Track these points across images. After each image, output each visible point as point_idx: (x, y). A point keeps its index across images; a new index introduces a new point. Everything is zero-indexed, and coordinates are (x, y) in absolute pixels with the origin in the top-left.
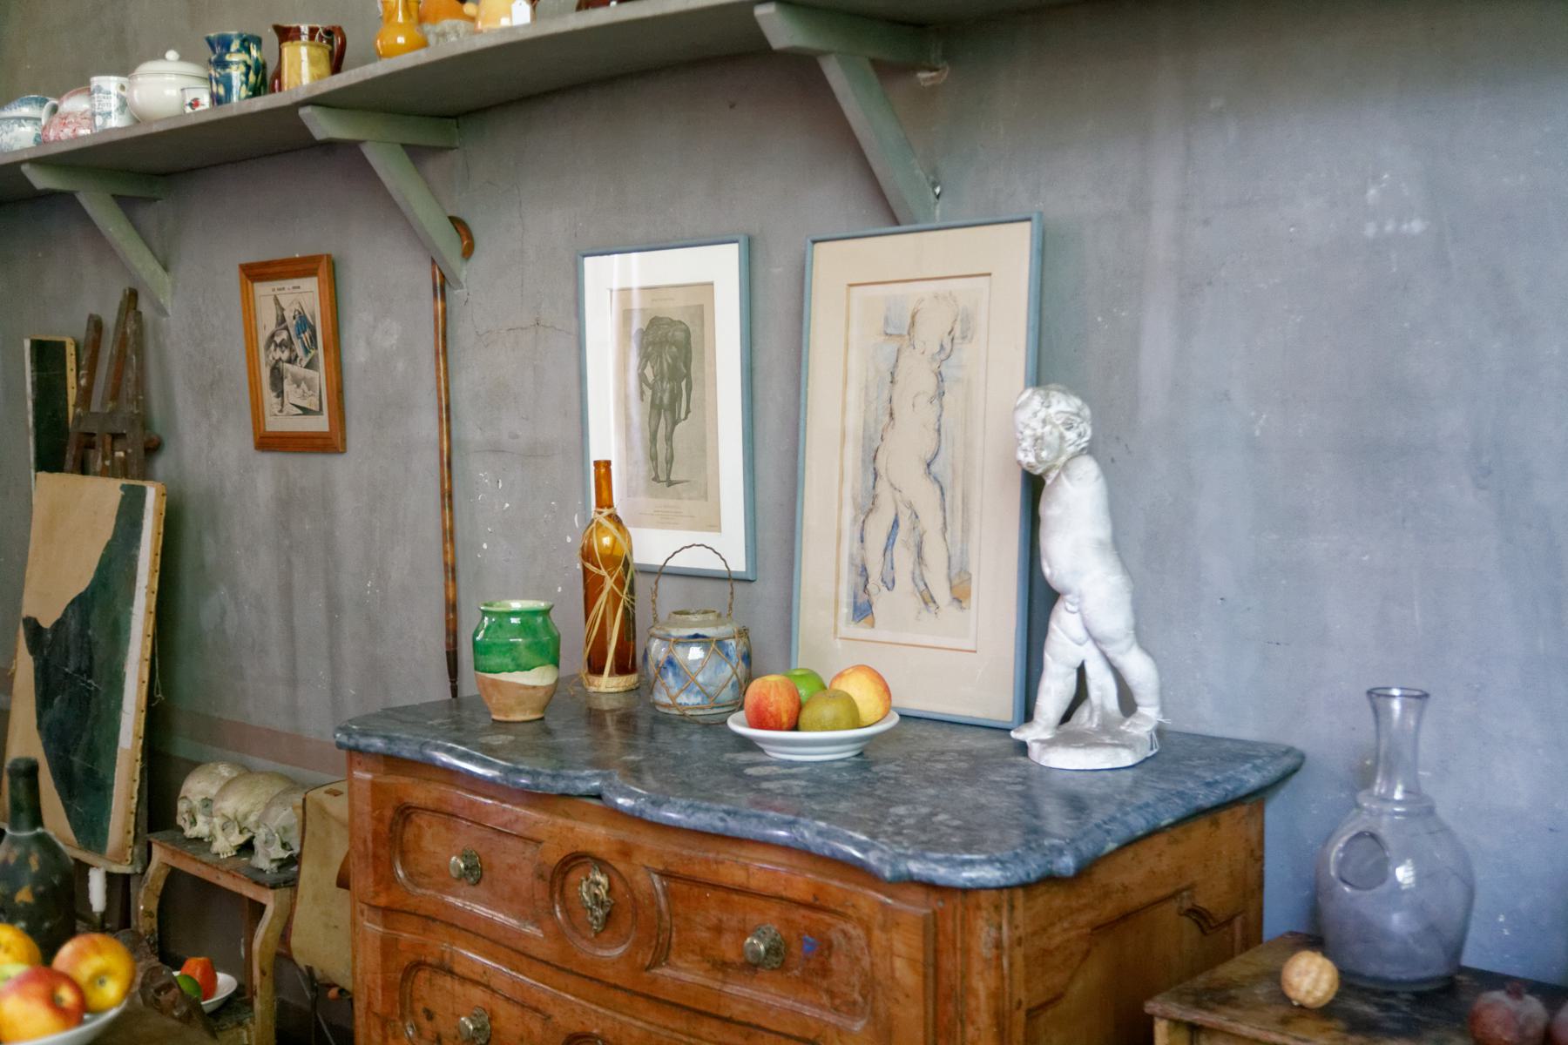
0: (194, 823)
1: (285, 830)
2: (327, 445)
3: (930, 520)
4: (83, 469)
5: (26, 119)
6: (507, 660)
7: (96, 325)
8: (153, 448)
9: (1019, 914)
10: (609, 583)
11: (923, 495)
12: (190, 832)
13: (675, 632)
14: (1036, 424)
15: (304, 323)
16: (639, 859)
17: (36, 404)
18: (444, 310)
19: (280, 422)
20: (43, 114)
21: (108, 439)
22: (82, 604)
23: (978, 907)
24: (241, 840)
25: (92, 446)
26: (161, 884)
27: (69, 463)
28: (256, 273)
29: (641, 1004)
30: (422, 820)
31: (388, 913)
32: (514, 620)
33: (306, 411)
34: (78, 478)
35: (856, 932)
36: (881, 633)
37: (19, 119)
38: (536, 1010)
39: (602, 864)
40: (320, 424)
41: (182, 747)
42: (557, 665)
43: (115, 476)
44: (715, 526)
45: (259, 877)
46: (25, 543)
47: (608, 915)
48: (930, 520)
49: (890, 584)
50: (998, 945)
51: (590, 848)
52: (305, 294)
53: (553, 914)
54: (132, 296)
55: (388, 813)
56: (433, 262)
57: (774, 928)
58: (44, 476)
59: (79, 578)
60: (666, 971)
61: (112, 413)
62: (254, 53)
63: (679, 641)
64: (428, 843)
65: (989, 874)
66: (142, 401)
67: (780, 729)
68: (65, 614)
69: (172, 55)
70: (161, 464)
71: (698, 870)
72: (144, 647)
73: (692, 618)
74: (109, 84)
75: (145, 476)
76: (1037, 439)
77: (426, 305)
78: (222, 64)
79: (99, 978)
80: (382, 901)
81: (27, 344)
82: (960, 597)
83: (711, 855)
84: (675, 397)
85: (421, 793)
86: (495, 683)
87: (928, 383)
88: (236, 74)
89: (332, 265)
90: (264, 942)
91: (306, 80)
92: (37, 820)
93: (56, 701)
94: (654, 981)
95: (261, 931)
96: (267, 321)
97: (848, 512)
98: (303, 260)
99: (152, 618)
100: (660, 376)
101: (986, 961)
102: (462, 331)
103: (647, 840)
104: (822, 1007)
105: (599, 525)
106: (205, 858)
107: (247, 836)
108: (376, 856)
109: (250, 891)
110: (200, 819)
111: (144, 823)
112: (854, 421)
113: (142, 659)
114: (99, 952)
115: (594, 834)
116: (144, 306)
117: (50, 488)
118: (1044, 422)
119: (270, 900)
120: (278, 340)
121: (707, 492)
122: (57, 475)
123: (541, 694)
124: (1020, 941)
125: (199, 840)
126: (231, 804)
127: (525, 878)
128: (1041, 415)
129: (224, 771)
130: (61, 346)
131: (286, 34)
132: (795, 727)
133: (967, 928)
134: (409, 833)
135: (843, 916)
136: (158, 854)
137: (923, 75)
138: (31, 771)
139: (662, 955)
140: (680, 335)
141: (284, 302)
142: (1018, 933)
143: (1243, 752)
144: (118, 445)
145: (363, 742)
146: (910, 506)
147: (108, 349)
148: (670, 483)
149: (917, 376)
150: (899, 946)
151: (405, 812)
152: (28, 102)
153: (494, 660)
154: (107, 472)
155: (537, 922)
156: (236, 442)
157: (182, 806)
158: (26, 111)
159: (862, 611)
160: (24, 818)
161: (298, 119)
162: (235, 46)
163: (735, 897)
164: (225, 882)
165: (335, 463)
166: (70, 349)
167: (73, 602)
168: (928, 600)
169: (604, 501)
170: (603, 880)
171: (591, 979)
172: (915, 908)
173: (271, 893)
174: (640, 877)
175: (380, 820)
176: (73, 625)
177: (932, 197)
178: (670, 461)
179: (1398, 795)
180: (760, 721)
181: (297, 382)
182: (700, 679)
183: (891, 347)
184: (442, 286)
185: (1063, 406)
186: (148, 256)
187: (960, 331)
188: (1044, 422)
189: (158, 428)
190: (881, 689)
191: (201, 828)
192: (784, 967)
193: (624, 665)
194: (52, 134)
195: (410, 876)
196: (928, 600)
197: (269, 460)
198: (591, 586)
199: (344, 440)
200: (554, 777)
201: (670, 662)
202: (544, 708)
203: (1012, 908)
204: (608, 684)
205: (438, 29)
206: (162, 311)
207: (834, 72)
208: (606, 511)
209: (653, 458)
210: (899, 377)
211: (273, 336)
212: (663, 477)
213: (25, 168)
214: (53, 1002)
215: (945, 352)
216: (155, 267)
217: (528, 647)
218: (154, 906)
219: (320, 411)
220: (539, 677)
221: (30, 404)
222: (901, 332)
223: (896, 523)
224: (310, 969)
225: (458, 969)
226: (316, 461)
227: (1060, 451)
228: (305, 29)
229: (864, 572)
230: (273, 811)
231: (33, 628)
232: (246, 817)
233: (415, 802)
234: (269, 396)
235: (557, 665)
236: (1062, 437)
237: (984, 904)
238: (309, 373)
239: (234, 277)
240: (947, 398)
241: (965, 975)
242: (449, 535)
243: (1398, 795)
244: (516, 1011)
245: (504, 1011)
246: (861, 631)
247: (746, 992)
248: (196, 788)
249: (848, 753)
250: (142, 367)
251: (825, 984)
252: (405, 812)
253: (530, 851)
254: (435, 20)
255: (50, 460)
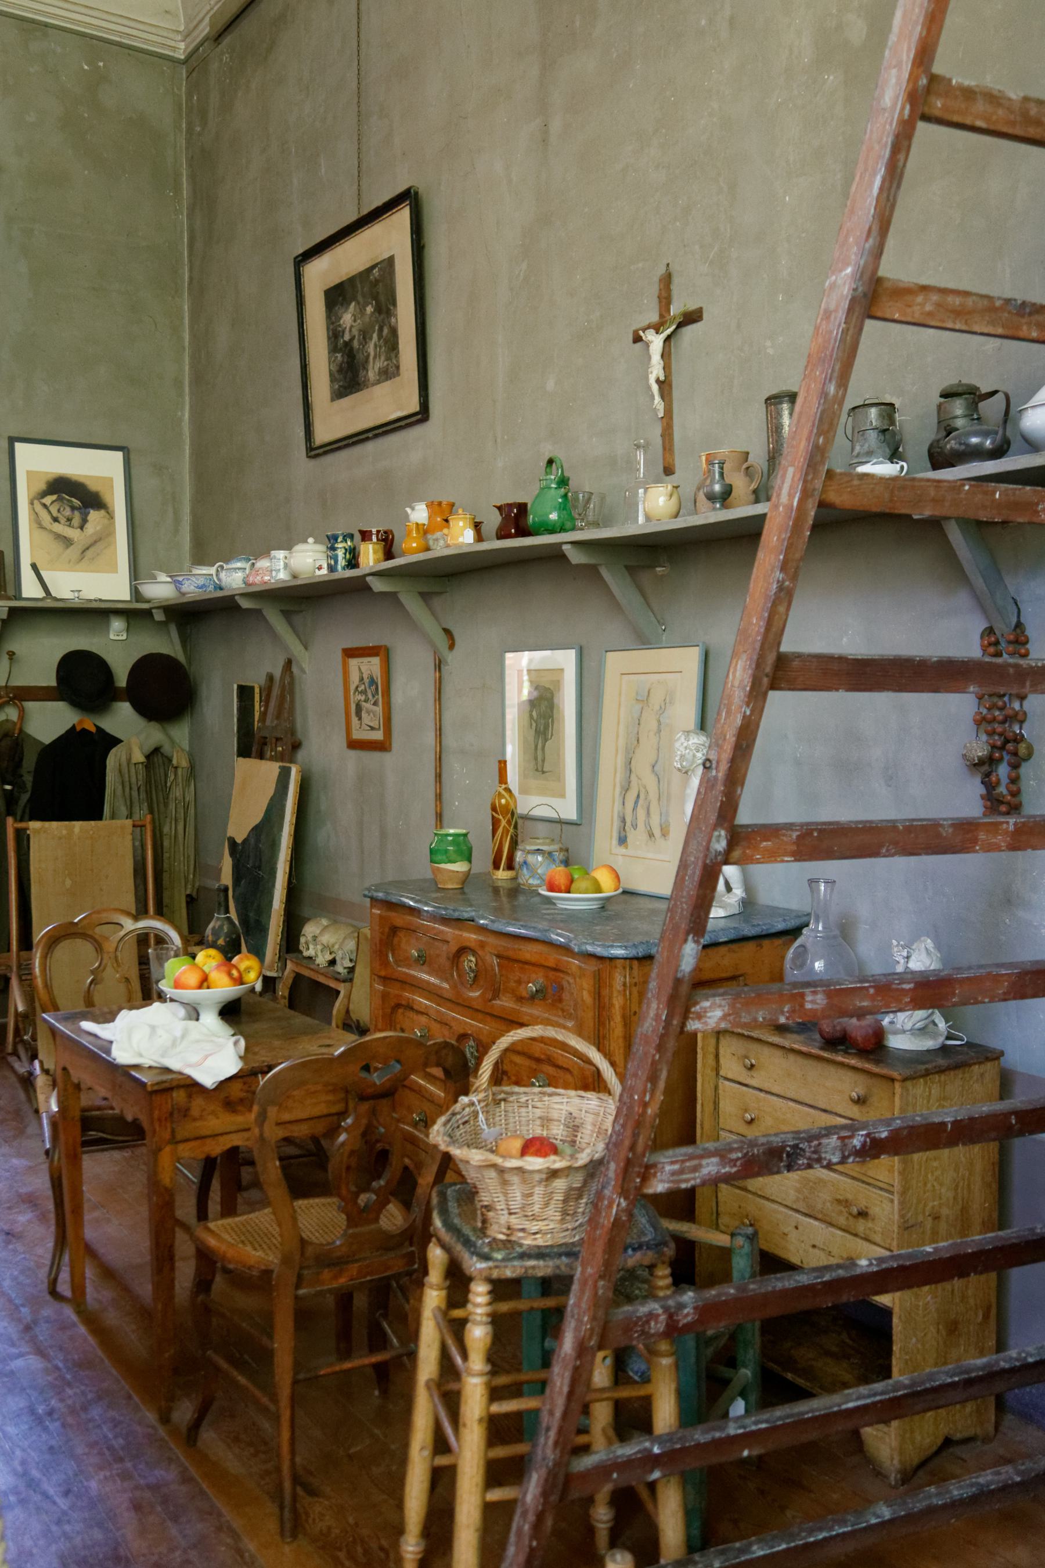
0: (308, 949)
1: (352, 952)
2: (382, 746)
3: (653, 796)
4: (261, 756)
5: (239, 569)
6: (444, 858)
7: (270, 678)
8: (296, 746)
9: (635, 972)
10: (504, 823)
11: (650, 781)
12: (306, 954)
13: (528, 848)
14: (682, 749)
15: (372, 681)
16: (487, 949)
17: (238, 720)
18: (440, 677)
19: (357, 735)
20: (248, 566)
21: (274, 740)
22: (257, 830)
23: (616, 967)
24: (330, 957)
25: (265, 744)
26: (290, 981)
27: (254, 754)
28: (350, 653)
29: (489, 1019)
30: (401, 934)
31: (385, 980)
32: (450, 838)
33: (372, 728)
34: (257, 761)
35: (571, 981)
36: (630, 851)
37: (235, 569)
38: (446, 1024)
39: (474, 953)
40: (378, 736)
41: (306, 911)
42: (470, 861)
43: (276, 761)
44: (562, 795)
45: (338, 976)
46: (230, 795)
47: (475, 976)
48: (653, 796)
49: (635, 826)
50: (624, 985)
51: (468, 944)
52: (372, 666)
53: (452, 976)
54: (289, 663)
55: (387, 930)
56: (435, 653)
57: (541, 980)
58: (241, 759)
59: (256, 817)
60: (497, 1002)
61: (277, 725)
62: (349, 543)
63: (529, 852)
64: (403, 945)
65: (619, 952)
66: (293, 723)
67: (560, 891)
68: (249, 836)
69: (311, 540)
70: (301, 755)
71: (510, 954)
72: (287, 854)
73: (538, 841)
74: (280, 554)
75: (291, 761)
76: (682, 756)
77: (431, 675)
78: (333, 549)
79: (248, 970)
80: (383, 973)
81: (235, 686)
82: (665, 834)
83: (516, 946)
84: (546, 727)
85: (399, 919)
86: (438, 869)
87: (654, 725)
88: (340, 553)
89: (387, 650)
90: (339, 1011)
91: (371, 564)
92: (227, 911)
93: (243, 882)
94: (493, 1005)
95: (337, 1004)
96: (354, 679)
97: (618, 790)
98: (373, 648)
99: (292, 839)
100: (540, 715)
101: (619, 991)
102: (448, 690)
103: (492, 940)
104: (559, 1016)
105: (500, 793)
106: (312, 966)
107: (333, 956)
108: (380, 951)
109: (333, 984)
110: (311, 947)
111: (284, 949)
112: (622, 742)
113: (286, 861)
114: (248, 959)
115: (471, 937)
116: (295, 669)
117: (243, 765)
118: (686, 748)
119: (342, 988)
120: (360, 689)
121: (560, 778)
122: (248, 759)
123: (461, 875)
124: (636, 984)
125: (310, 958)
126: (326, 938)
127: (443, 961)
128: (685, 744)
129: (324, 922)
130: (252, 688)
131: (365, 536)
132: (569, 892)
133: (611, 977)
134: (396, 940)
135: (567, 973)
136: (290, 965)
137: (658, 569)
138: (226, 890)
139: (496, 995)
140: (549, 695)
141: (363, 669)
142: (635, 980)
143: (785, 913)
144: (279, 743)
145: (375, 894)
146: (645, 787)
147: (276, 691)
148: (543, 772)
149: (650, 723)
150: (585, 986)
151: (394, 930)
152: (240, 560)
153: (439, 857)
154: (272, 759)
155: (447, 980)
156: (339, 741)
157: (302, 940)
158: (239, 565)
159: (622, 841)
160: (222, 909)
161: (366, 582)
162: (340, 540)
163: (527, 966)
164: (322, 979)
165: (386, 757)
166: (257, 690)
167: (253, 829)
168: (651, 835)
169: (502, 778)
170: (473, 959)
171: (466, 1007)
172: (592, 967)
173: (342, 985)
174: (488, 958)
175: (382, 933)
176: (252, 841)
177: (660, 631)
178: (543, 761)
179: (820, 928)
180: (551, 889)
181: (368, 712)
182: (539, 871)
183: (638, 707)
184: (439, 665)
185: (696, 741)
186: (297, 642)
187: (668, 701)
188: (686, 748)
189: (299, 735)
190: (613, 876)
191: (311, 952)
192: (544, 999)
193: (510, 867)
194: (251, 580)
195: (396, 961)
196: (651, 835)
197: (353, 754)
198: (495, 823)
199: (390, 744)
200: (454, 911)
201: (525, 862)
202: (463, 882)
203: (631, 968)
204: (502, 874)
205: (435, 537)
206: (303, 671)
207: (604, 572)
208: (504, 786)
209: (536, 759)
210: (642, 722)
211: (357, 687)
212: (540, 769)
213: (237, 598)
214: (230, 975)
215: (662, 710)
216: (301, 648)
217: (455, 851)
218: (286, 994)
219: (379, 729)
220: (460, 867)
221: (235, 720)
222: (643, 699)
223: (638, 796)
224: (358, 1021)
225: (415, 1007)
226: (376, 755)
227: (693, 762)
228: (374, 531)
229: (624, 821)
230: (346, 941)
231: (233, 843)
232: (333, 946)
233: (398, 925)
234: (354, 719)
235: (470, 861)
236: (694, 756)
237: (619, 966)
238: (375, 708)
239: (339, 654)
240: (662, 733)
241: (610, 998)
242: (439, 797)
243: (820, 928)
244: (438, 1026)
245: (435, 1027)
246: (622, 850)
247: (529, 1011)
248: (310, 930)
249: (594, 906)
250: (292, 701)
251: (560, 1005)
252: (394, 930)
253: (445, 947)
254: (433, 533)
255: (244, 752)
